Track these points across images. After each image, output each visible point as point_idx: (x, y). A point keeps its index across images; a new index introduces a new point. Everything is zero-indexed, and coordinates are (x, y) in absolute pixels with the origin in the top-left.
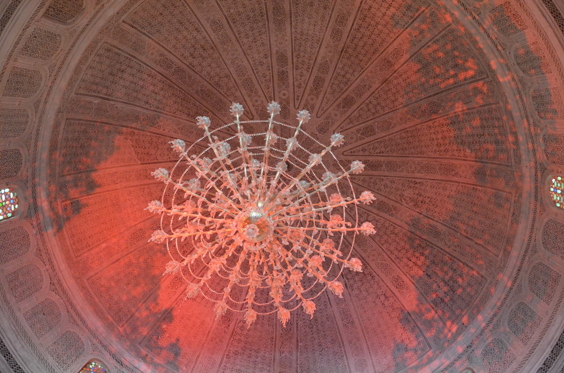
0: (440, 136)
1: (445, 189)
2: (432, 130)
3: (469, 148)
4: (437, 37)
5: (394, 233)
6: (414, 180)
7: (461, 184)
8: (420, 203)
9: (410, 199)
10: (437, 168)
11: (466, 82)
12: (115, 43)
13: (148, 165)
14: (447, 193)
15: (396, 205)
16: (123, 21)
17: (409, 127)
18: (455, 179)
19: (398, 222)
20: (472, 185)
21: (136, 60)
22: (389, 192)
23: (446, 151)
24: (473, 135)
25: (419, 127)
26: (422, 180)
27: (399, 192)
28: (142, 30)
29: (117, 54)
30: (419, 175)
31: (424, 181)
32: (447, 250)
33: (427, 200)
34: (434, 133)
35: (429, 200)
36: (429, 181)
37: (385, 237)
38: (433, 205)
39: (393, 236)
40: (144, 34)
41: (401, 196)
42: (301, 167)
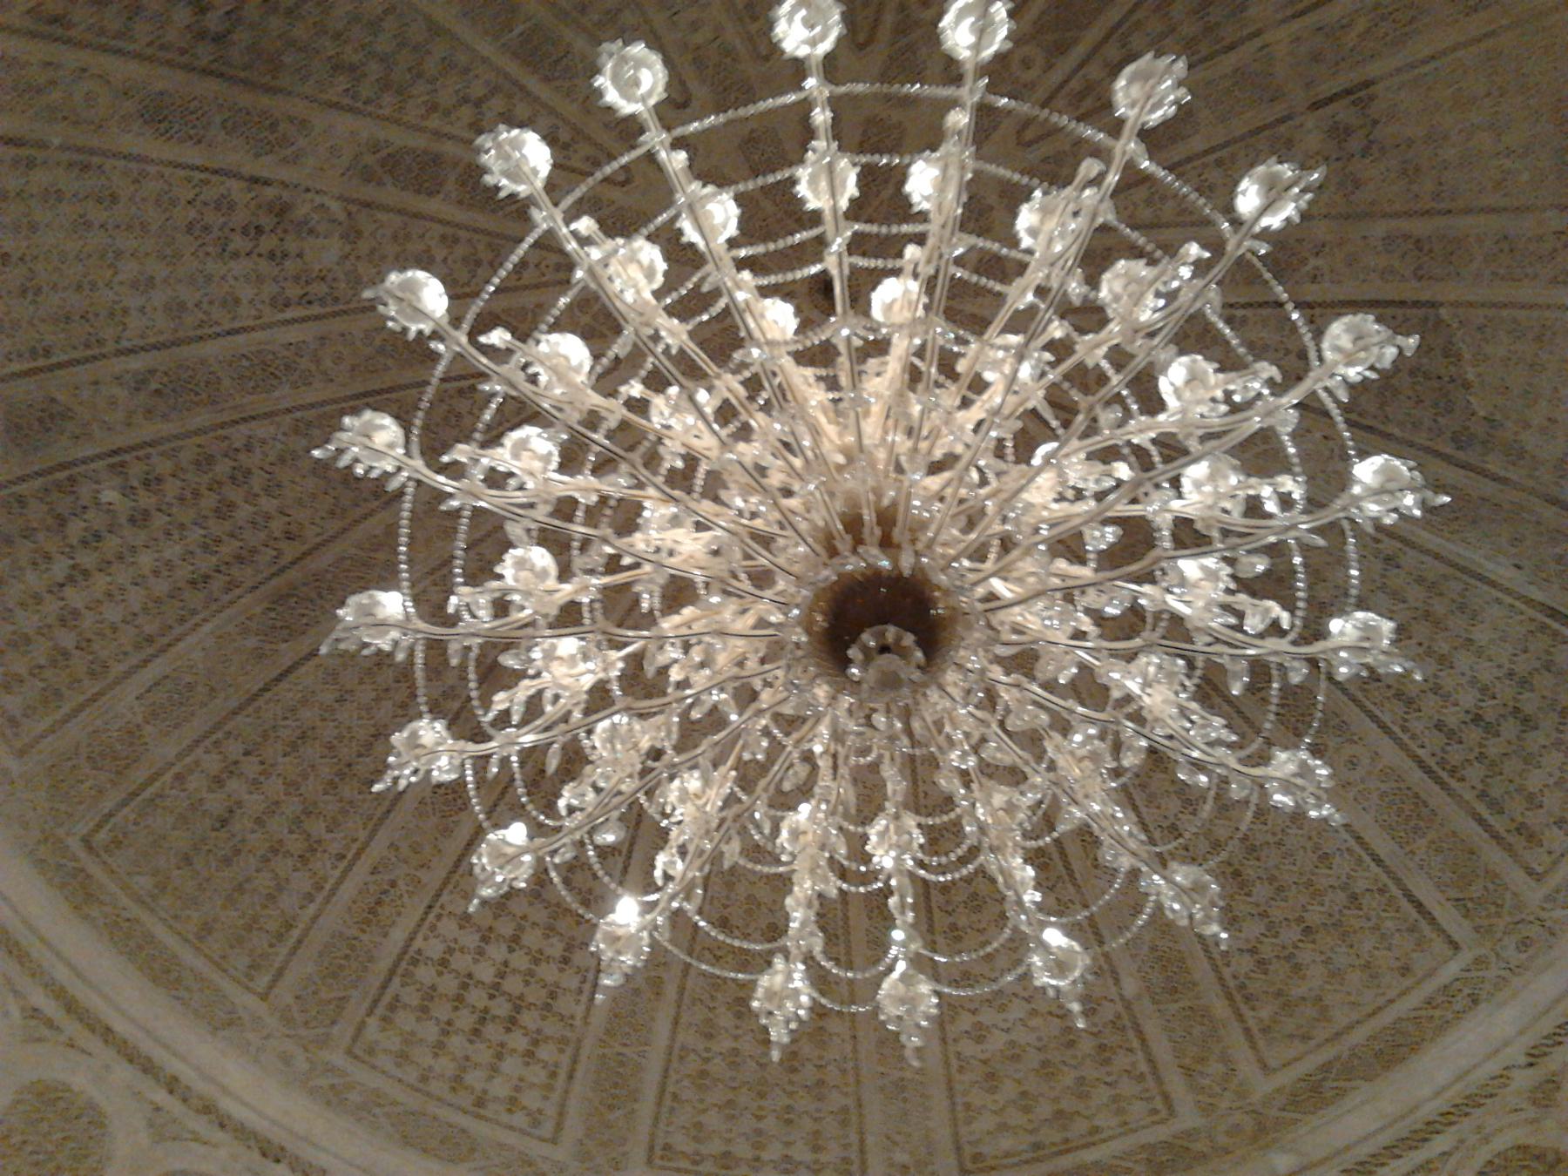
0: (244, 512)
1: (177, 308)
2: (277, 526)
3: (109, 509)
4: (312, 909)
5: (352, 68)
6: (316, 310)
7: (110, 347)
8: (267, 221)
9: (311, 231)
10: (226, 382)
11: (176, 769)
12: (1494, 856)
13: (1409, 296)
14: (159, 297)
15: (369, 192)
16: (1455, 946)
17: (371, 513)
18: (136, 364)
19: (344, 123)
20: (60, 366)
21: (1420, 752)
22: (408, 237)
23: (205, 461)
24: (105, 566)
25: (333, 526)
26: (280, 316)
27: (364, 246)
28: (1384, 878)
29: (1497, 807)
30: (293, 334)
31: (270, 315)
32: (85, 57)
33: (238, 242)
34: (268, 517)
35: (231, 247)
36: (251, 323)
37: (384, 44)
38: (206, 228)
39: (351, 56)
40: (1378, 861)
41: (352, 234)
42: (743, 967)
